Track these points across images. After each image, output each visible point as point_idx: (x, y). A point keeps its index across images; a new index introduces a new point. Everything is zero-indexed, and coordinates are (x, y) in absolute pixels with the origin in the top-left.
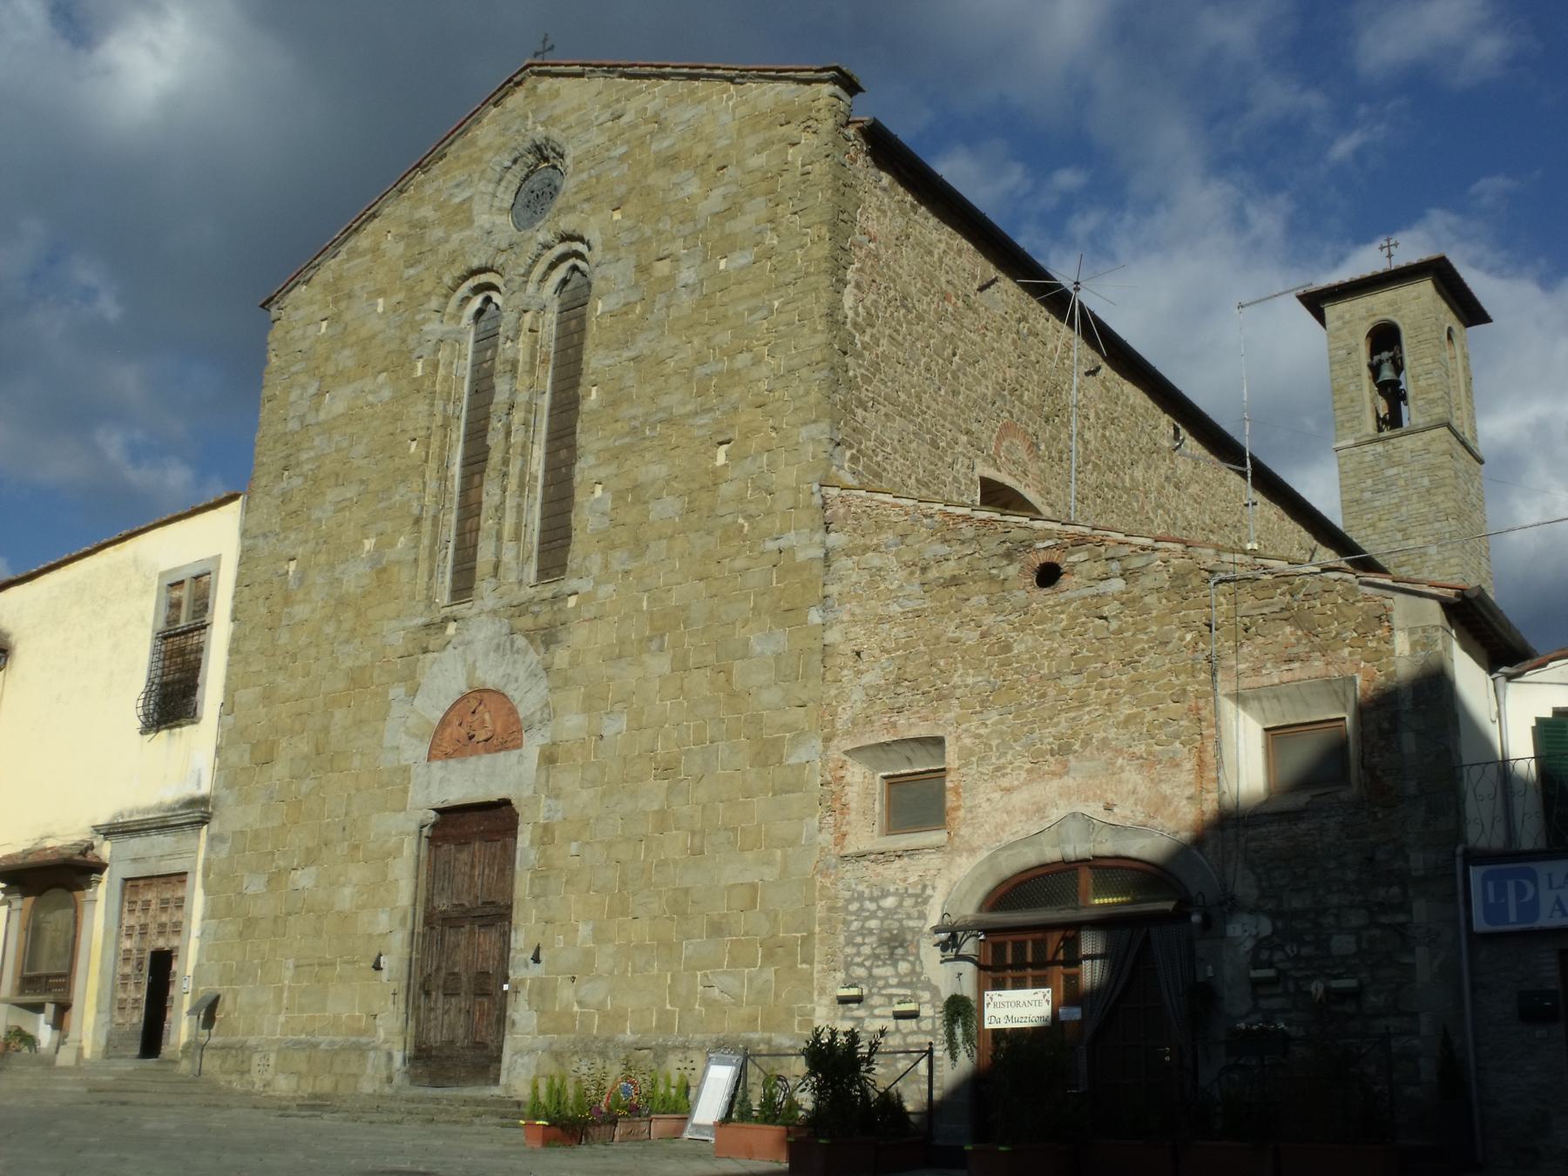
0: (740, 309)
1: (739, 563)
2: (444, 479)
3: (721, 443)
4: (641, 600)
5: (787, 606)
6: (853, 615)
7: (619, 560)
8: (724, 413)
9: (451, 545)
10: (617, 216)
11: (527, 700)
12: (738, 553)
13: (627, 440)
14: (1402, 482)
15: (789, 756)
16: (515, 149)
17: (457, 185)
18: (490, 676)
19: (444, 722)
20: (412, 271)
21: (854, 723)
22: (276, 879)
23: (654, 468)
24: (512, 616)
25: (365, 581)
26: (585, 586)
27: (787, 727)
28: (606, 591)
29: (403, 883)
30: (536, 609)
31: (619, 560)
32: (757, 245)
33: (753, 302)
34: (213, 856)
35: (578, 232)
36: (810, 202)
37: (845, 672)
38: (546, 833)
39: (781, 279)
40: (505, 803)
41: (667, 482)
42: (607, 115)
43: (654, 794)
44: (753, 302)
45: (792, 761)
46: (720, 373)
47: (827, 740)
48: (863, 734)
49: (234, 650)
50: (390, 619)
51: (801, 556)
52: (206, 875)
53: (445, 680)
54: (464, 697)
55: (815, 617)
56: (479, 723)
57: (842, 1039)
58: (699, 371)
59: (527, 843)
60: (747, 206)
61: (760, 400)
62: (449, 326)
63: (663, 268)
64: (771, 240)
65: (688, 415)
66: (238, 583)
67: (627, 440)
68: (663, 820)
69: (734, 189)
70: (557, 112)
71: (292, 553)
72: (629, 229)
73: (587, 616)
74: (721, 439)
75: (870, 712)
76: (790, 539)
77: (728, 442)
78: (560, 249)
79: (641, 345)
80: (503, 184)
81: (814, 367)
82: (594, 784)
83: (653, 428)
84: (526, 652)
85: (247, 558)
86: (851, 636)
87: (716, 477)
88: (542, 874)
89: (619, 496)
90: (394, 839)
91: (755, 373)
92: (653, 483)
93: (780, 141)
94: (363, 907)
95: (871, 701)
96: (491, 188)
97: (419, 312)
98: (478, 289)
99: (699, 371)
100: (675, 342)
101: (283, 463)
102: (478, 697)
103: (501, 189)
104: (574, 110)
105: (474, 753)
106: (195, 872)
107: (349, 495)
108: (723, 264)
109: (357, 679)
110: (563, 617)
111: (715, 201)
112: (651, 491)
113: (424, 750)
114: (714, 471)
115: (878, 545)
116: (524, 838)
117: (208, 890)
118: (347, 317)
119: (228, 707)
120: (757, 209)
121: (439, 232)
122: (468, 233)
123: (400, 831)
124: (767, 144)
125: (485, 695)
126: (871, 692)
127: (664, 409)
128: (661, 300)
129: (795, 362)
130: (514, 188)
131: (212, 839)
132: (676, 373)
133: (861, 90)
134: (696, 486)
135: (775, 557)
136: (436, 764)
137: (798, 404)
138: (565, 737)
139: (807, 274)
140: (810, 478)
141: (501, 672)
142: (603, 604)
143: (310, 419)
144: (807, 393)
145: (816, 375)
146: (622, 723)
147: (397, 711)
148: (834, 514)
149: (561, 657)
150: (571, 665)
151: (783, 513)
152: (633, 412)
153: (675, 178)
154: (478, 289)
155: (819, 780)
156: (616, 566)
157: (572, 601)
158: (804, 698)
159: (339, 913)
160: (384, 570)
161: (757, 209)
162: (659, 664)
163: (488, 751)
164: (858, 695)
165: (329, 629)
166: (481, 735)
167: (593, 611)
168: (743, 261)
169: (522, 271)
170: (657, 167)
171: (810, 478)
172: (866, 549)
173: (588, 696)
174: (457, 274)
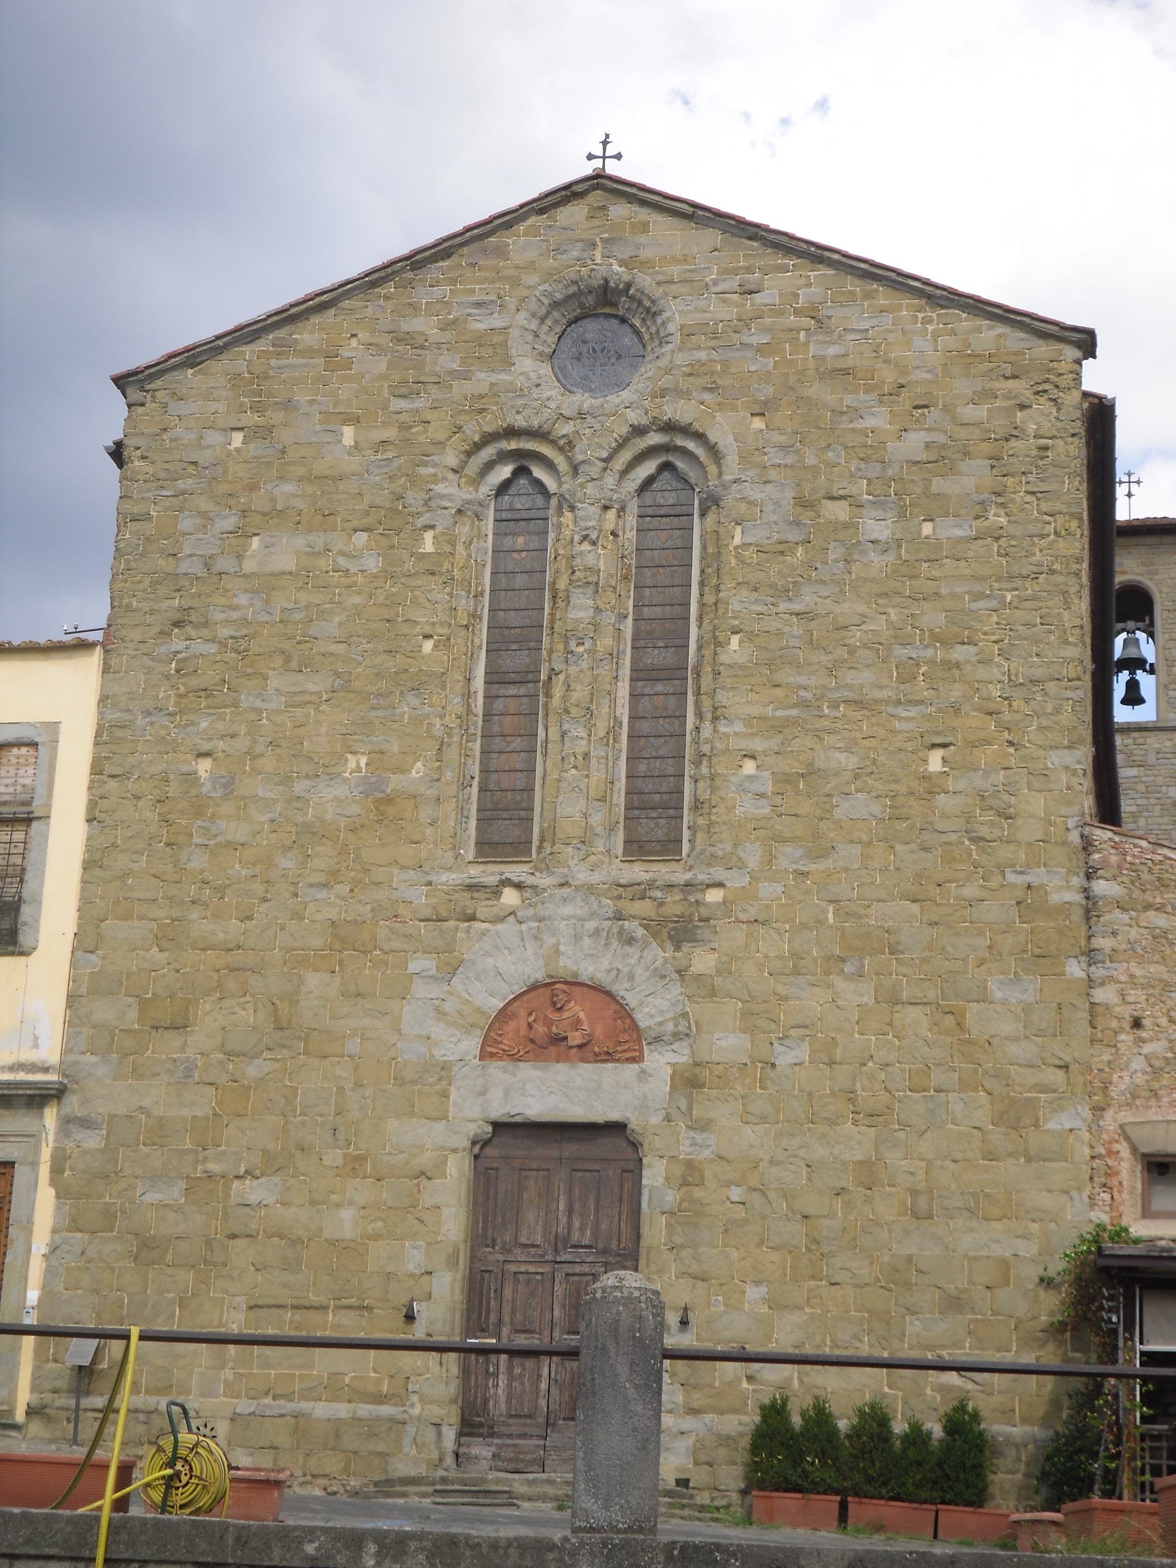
0: (958, 590)
1: (969, 891)
2: (468, 696)
3: (934, 746)
4: (825, 912)
5: (1038, 951)
6: (1132, 976)
7: (788, 857)
8: (939, 710)
9: (475, 783)
10: (758, 424)
11: (653, 1007)
12: (968, 880)
13: (794, 712)
14: (1141, 787)
15: (1046, 1121)
16: (574, 283)
17: (479, 305)
18: (592, 966)
19: (504, 1015)
20: (402, 404)
21: (1135, 1097)
22: (203, 1188)
23: (841, 756)
24: (619, 897)
25: (355, 809)
26: (737, 881)
27: (1046, 1089)
28: (769, 890)
29: (447, 1212)
30: (658, 894)
31: (788, 857)
32: (977, 517)
33: (977, 587)
34: (70, 1145)
35: (697, 426)
36: (1053, 486)
37: (1122, 1037)
38: (690, 1175)
39: (1016, 569)
40: (618, 1128)
41: (856, 777)
42: (733, 283)
43: (855, 1142)
44: (977, 587)
45: (1052, 1125)
46: (932, 662)
47: (1099, 1110)
48: (1148, 1107)
49: (93, 863)
50: (403, 868)
51: (1055, 898)
52: (57, 1170)
53: (503, 963)
54: (534, 988)
55: (1075, 969)
56: (553, 1019)
57: (936, 1430)
58: (901, 652)
59: (660, 1181)
60: (962, 466)
61: (992, 706)
62: (467, 494)
63: (838, 511)
64: (997, 518)
65: (887, 702)
66: (97, 768)
67: (794, 712)
68: (869, 1173)
69: (941, 438)
70: (645, 254)
71: (206, 747)
72: (782, 448)
73: (743, 917)
74: (939, 740)
75: (1156, 1085)
76: (1037, 876)
77: (944, 746)
78: (654, 439)
79: (808, 599)
80: (549, 322)
81: (1065, 683)
82: (763, 1119)
83: (835, 706)
84: (646, 945)
85: (107, 737)
86: (1130, 999)
87: (932, 786)
88: (686, 1216)
89: (784, 780)
90: (428, 1155)
91: (982, 673)
92: (837, 774)
93: (1007, 397)
94: (377, 1237)
95: (1156, 1072)
96: (534, 325)
97: (425, 464)
98: (504, 457)
99: (901, 652)
100: (861, 608)
101: (178, 616)
102: (553, 990)
103: (545, 328)
104: (675, 260)
105: (565, 1058)
106: (34, 1165)
107: (311, 687)
108: (927, 529)
109: (344, 940)
110: (704, 912)
111: (914, 443)
112: (834, 782)
113: (471, 1044)
114: (926, 777)
115: (1163, 905)
116: (654, 1175)
117: (62, 1193)
118: (285, 436)
119: (86, 941)
120: (972, 477)
121: (450, 362)
122: (504, 377)
123: (439, 1145)
124: (987, 395)
125: (577, 991)
126: (1157, 1064)
127: (850, 687)
128: (835, 552)
129: (1039, 673)
130: (559, 329)
131: (66, 1122)
132: (865, 646)
133: (1095, 357)
134: (903, 789)
135: (1019, 894)
136: (495, 1069)
137: (1045, 723)
138: (715, 1057)
139: (1052, 572)
140: (1064, 811)
141: (605, 963)
142: (769, 907)
143: (222, 564)
144: (1057, 711)
145: (1069, 694)
146: (802, 1053)
147: (422, 990)
148: (1105, 860)
149: (703, 961)
150: (719, 972)
151: (1029, 844)
152: (802, 680)
153: (849, 400)
154: (504, 457)
155: (1087, 1152)
156: (783, 863)
157: (714, 896)
158: (1067, 1058)
159: (331, 1243)
160: (389, 800)
161: (972, 477)
162: (855, 994)
163: (584, 1060)
164: (1138, 1064)
165: (288, 862)
166: (575, 1038)
167: (753, 912)
168: (958, 532)
169: (605, 455)
170: (822, 377)
171: (1064, 811)
172: (1148, 907)
173: (746, 1014)
174: (489, 429)
